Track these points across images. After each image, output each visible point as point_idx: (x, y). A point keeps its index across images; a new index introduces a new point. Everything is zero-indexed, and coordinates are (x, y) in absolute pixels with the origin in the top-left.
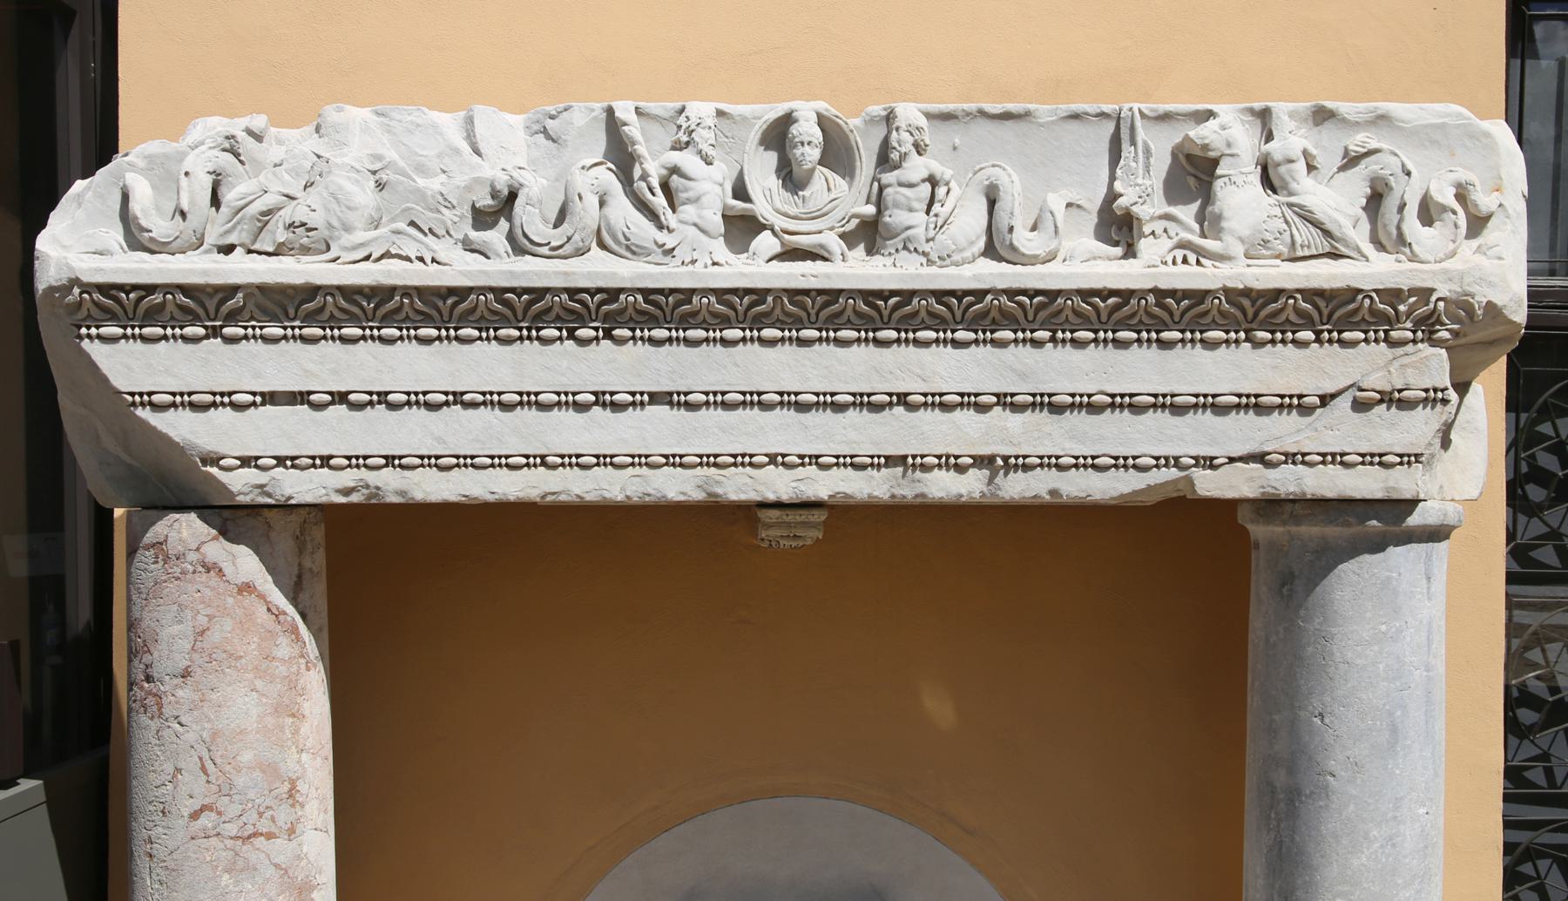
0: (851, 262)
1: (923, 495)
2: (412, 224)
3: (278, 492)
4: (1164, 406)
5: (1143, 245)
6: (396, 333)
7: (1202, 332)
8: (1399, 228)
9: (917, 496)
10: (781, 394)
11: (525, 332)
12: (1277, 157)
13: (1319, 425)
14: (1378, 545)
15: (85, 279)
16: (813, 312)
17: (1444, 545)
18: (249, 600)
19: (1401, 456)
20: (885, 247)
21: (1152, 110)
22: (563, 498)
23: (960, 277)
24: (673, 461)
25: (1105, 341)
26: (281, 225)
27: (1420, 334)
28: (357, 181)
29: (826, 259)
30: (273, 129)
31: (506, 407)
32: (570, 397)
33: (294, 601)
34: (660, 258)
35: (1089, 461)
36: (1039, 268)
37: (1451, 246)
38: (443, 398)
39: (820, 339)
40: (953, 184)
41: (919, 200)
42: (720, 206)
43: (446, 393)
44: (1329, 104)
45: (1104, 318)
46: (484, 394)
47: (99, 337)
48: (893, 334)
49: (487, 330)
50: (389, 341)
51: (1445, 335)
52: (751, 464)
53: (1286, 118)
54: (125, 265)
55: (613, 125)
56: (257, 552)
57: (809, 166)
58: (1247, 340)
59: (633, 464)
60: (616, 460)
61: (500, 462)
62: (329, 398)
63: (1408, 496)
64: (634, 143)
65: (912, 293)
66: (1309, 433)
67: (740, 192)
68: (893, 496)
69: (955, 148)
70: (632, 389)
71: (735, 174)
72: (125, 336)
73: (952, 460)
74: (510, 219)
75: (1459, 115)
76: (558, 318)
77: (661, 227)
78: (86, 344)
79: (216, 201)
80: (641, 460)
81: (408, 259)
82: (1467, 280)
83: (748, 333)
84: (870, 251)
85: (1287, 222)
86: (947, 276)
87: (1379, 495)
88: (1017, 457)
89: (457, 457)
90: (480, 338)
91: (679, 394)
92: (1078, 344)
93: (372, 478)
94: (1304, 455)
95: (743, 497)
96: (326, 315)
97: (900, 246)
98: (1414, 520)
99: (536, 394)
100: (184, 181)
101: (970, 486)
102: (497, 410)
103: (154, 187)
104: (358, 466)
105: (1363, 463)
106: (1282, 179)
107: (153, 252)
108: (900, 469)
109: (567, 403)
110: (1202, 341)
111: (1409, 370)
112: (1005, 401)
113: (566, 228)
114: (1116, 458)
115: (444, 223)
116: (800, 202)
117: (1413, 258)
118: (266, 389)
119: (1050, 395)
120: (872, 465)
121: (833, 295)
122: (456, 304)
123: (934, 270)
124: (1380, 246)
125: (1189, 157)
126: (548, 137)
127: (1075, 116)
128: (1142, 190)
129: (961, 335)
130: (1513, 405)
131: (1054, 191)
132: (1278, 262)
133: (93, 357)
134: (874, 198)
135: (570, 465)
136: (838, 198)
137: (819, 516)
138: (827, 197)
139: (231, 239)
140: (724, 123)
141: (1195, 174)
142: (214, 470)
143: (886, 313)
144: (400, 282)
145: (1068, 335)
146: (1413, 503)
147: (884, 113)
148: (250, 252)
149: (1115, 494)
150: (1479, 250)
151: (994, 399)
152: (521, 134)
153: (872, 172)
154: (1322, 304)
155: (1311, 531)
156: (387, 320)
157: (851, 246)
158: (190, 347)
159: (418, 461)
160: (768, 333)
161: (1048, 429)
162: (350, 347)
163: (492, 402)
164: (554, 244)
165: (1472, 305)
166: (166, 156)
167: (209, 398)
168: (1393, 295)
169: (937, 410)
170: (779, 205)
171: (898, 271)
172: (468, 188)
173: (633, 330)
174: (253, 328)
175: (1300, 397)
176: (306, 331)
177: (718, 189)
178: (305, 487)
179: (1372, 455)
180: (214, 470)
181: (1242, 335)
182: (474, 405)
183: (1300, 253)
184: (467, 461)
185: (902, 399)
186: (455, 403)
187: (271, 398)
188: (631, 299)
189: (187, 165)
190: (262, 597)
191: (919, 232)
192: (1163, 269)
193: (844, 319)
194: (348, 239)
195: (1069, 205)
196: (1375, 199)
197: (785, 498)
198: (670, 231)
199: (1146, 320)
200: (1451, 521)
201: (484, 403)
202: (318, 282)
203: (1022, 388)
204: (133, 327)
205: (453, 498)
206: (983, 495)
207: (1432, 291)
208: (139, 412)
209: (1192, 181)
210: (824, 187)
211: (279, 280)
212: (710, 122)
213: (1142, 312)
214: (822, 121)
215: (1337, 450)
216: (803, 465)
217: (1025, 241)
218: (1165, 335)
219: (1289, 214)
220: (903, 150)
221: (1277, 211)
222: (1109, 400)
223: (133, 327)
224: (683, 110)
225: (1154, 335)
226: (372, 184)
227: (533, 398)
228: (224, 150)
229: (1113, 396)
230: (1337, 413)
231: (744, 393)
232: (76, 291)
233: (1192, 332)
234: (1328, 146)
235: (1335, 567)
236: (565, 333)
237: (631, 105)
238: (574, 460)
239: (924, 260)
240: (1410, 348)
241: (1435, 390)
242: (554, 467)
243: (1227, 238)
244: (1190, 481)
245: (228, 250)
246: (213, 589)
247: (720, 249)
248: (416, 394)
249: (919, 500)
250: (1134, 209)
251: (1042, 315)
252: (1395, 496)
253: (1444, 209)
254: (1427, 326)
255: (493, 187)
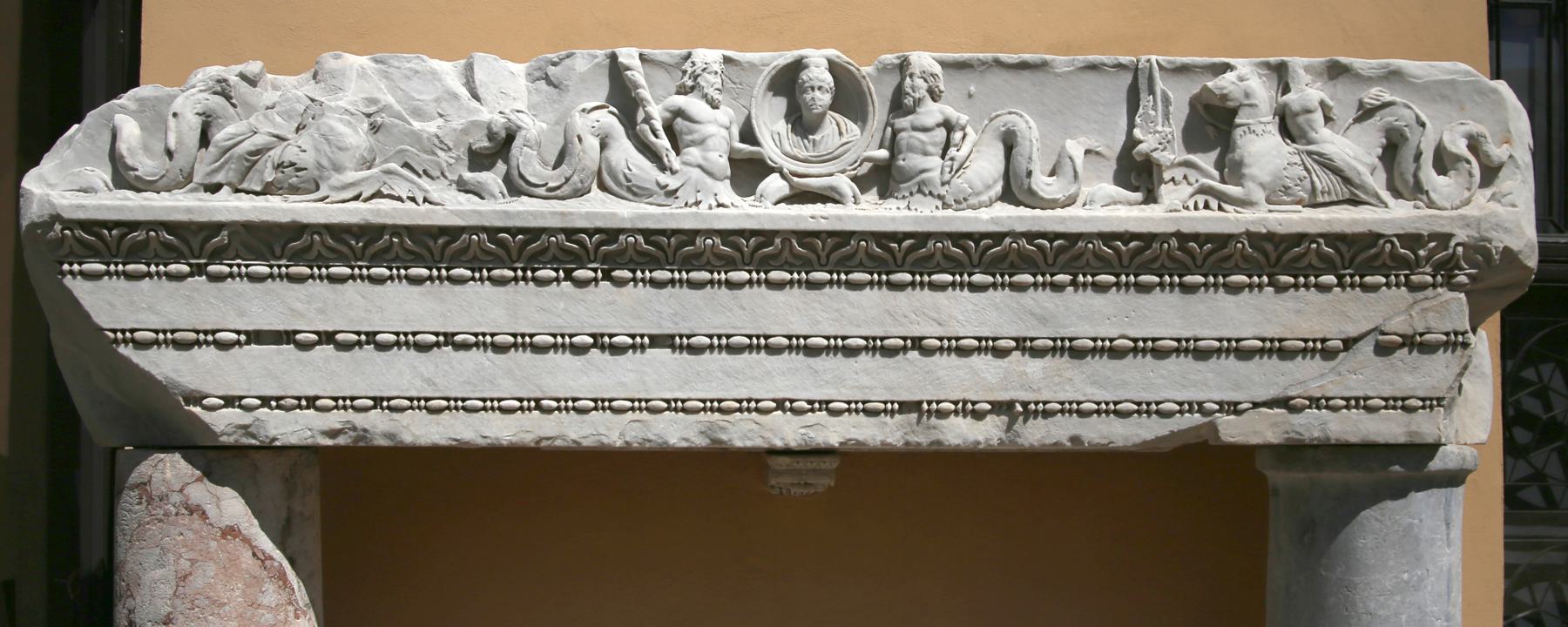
0: (863, 205)
1: (939, 442)
2: (406, 165)
3: (262, 433)
4: (1187, 351)
5: (1165, 190)
6: (386, 272)
7: (1224, 276)
8: (1415, 176)
9: (932, 443)
10: (789, 337)
11: (520, 273)
12: (1296, 107)
13: (1342, 369)
14: (1399, 491)
15: (66, 215)
16: (823, 255)
17: (1460, 490)
18: (234, 544)
19: (1423, 400)
20: (898, 190)
21: (1169, 62)
22: (558, 443)
23: (977, 219)
24: (676, 406)
25: (1171, 285)
26: (269, 165)
27: (1439, 278)
28: (350, 123)
29: (836, 202)
30: (270, 76)
31: (500, 349)
32: (567, 340)
33: (281, 545)
34: (662, 199)
35: (1112, 406)
36: (1059, 212)
37: (1467, 194)
38: (433, 338)
39: (831, 282)
40: (969, 130)
41: (935, 144)
42: (725, 147)
43: (437, 334)
44: (1343, 60)
45: (1126, 261)
46: (476, 335)
47: (81, 273)
48: (907, 277)
49: (480, 270)
50: (379, 281)
51: (1463, 279)
52: (757, 410)
53: (1302, 72)
54: (108, 202)
55: (616, 70)
56: (243, 495)
57: (820, 110)
58: (1270, 284)
59: (633, 409)
60: (615, 404)
61: (493, 405)
62: (315, 337)
63: (1430, 440)
64: (637, 86)
65: (927, 236)
66: (1332, 377)
67: (748, 135)
68: (907, 443)
69: (970, 96)
70: (632, 332)
71: (743, 119)
72: (108, 273)
73: (969, 406)
74: (506, 161)
75: (1467, 73)
76: (555, 259)
77: (663, 168)
78: (68, 280)
79: (205, 141)
80: (643, 405)
81: (399, 199)
82: (1484, 225)
83: (754, 275)
84: (884, 195)
85: (1306, 169)
86: (964, 219)
87: (1402, 440)
88: (1036, 403)
89: (448, 399)
90: (473, 279)
91: (681, 337)
92: (1100, 288)
93: (359, 419)
94: (1328, 399)
95: (749, 444)
96: (314, 254)
97: (915, 189)
98: (1436, 464)
99: (531, 336)
100: (172, 122)
101: (987, 432)
102: (490, 353)
103: (142, 128)
104: (345, 408)
105: (1386, 407)
106: (1301, 129)
107: (138, 190)
108: (914, 416)
109: (563, 345)
110: (1224, 285)
111: (1431, 314)
112: (1025, 346)
113: (565, 169)
114: (1139, 404)
115: (439, 164)
116: (810, 146)
117: (1431, 204)
118: (250, 328)
119: (1071, 340)
120: (885, 411)
121: (844, 237)
122: (448, 244)
123: (950, 212)
124: (1397, 194)
125: (1207, 107)
126: (549, 82)
127: (1093, 67)
128: (1160, 136)
129: (978, 278)
130: (1505, 356)
131: (1072, 138)
132: (1299, 207)
133: (76, 293)
134: (887, 143)
135: (567, 409)
136: (849, 142)
137: (831, 463)
138: (837, 141)
139: (219, 178)
140: (732, 71)
141: (1213, 124)
142: (197, 410)
143: (899, 256)
144: (389, 221)
145: (1089, 278)
146: (1433, 448)
147: (897, 62)
148: (237, 191)
149: (1137, 440)
150: (1493, 197)
151: (1013, 344)
152: (523, 81)
153: (885, 118)
154: (1343, 248)
155: (1335, 477)
156: (375, 260)
157: (863, 191)
158: (174, 284)
159: (407, 403)
160: (775, 275)
161: (1068, 374)
162: (339, 287)
163: (484, 344)
164: (552, 184)
165: (1489, 250)
166: (156, 98)
167: (193, 336)
168: (1413, 240)
169: (953, 355)
170: (788, 148)
171: (913, 213)
172: (465, 131)
173: (634, 272)
174: (239, 266)
175: (1324, 341)
176: (293, 270)
177: (724, 132)
178: (290, 429)
179: (1395, 399)
180: (197, 410)
181: (1265, 279)
182: (465, 346)
183: (1320, 199)
184: (458, 404)
185: (917, 343)
186: (446, 344)
187: (256, 337)
188: (631, 239)
189: (177, 105)
190: (247, 541)
191: (935, 175)
192: (1185, 213)
193: (857, 260)
194: (337, 179)
195: (1087, 152)
196: (1392, 149)
197: (793, 444)
198: (673, 172)
199: (1168, 263)
200: (1468, 466)
201: (477, 345)
202: (305, 221)
203: (1042, 334)
204: (116, 264)
205: (443, 442)
206: (1002, 442)
207: (1450, 236)
208: (122, 349)
209: (1210, 130)
210: (835, 131)
211: (265, 218)
212: (716, 67)
213: (1164, 256)
214: (833, 67)
215: (1360, 394)
216: (812, 410)
217: (1044, 185)
218: (1188, 279)
219: (1309, 162)
220: (917, 95)
221: (1297, 159)
222: (1131, 344)
223: (116, 264)
224: (689, 56)
225: (1176, 279)
226: (366, 126)
227: (527, 339)
228: (215, 93)
229: (1135, 340)
230: (1360, 357)
231: (750, 337)
232: (58, 227)
233: (1215, 276)
234: (1345, 100)
235: (1357, 513)
236: (562, 274)
237: (635, 52)
238: (496, 404)
239: (939, 204)
240: (1429, 292)
241: (1456, 334)
242: (549, 411)
243: (1250, 185)
244: (1213, 427)
245: (214, 188)
246: (196, 532)
247: (725, 192)
248: (406, 334)
249: (934, 447)
250: (1155, 155)
251: (1062, 259)
252: (1418, 441)
253: (1458, 158)
254: (1446, 270)
255: (489, 128)
